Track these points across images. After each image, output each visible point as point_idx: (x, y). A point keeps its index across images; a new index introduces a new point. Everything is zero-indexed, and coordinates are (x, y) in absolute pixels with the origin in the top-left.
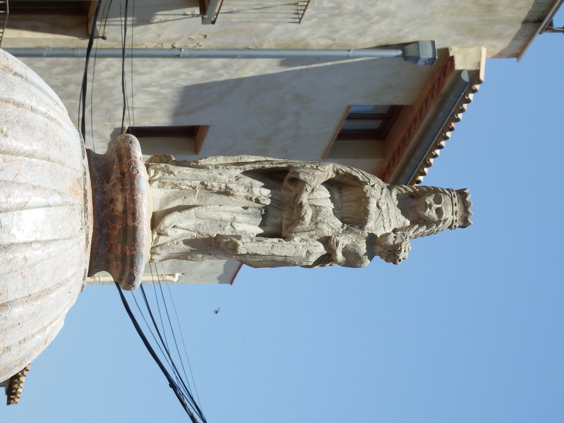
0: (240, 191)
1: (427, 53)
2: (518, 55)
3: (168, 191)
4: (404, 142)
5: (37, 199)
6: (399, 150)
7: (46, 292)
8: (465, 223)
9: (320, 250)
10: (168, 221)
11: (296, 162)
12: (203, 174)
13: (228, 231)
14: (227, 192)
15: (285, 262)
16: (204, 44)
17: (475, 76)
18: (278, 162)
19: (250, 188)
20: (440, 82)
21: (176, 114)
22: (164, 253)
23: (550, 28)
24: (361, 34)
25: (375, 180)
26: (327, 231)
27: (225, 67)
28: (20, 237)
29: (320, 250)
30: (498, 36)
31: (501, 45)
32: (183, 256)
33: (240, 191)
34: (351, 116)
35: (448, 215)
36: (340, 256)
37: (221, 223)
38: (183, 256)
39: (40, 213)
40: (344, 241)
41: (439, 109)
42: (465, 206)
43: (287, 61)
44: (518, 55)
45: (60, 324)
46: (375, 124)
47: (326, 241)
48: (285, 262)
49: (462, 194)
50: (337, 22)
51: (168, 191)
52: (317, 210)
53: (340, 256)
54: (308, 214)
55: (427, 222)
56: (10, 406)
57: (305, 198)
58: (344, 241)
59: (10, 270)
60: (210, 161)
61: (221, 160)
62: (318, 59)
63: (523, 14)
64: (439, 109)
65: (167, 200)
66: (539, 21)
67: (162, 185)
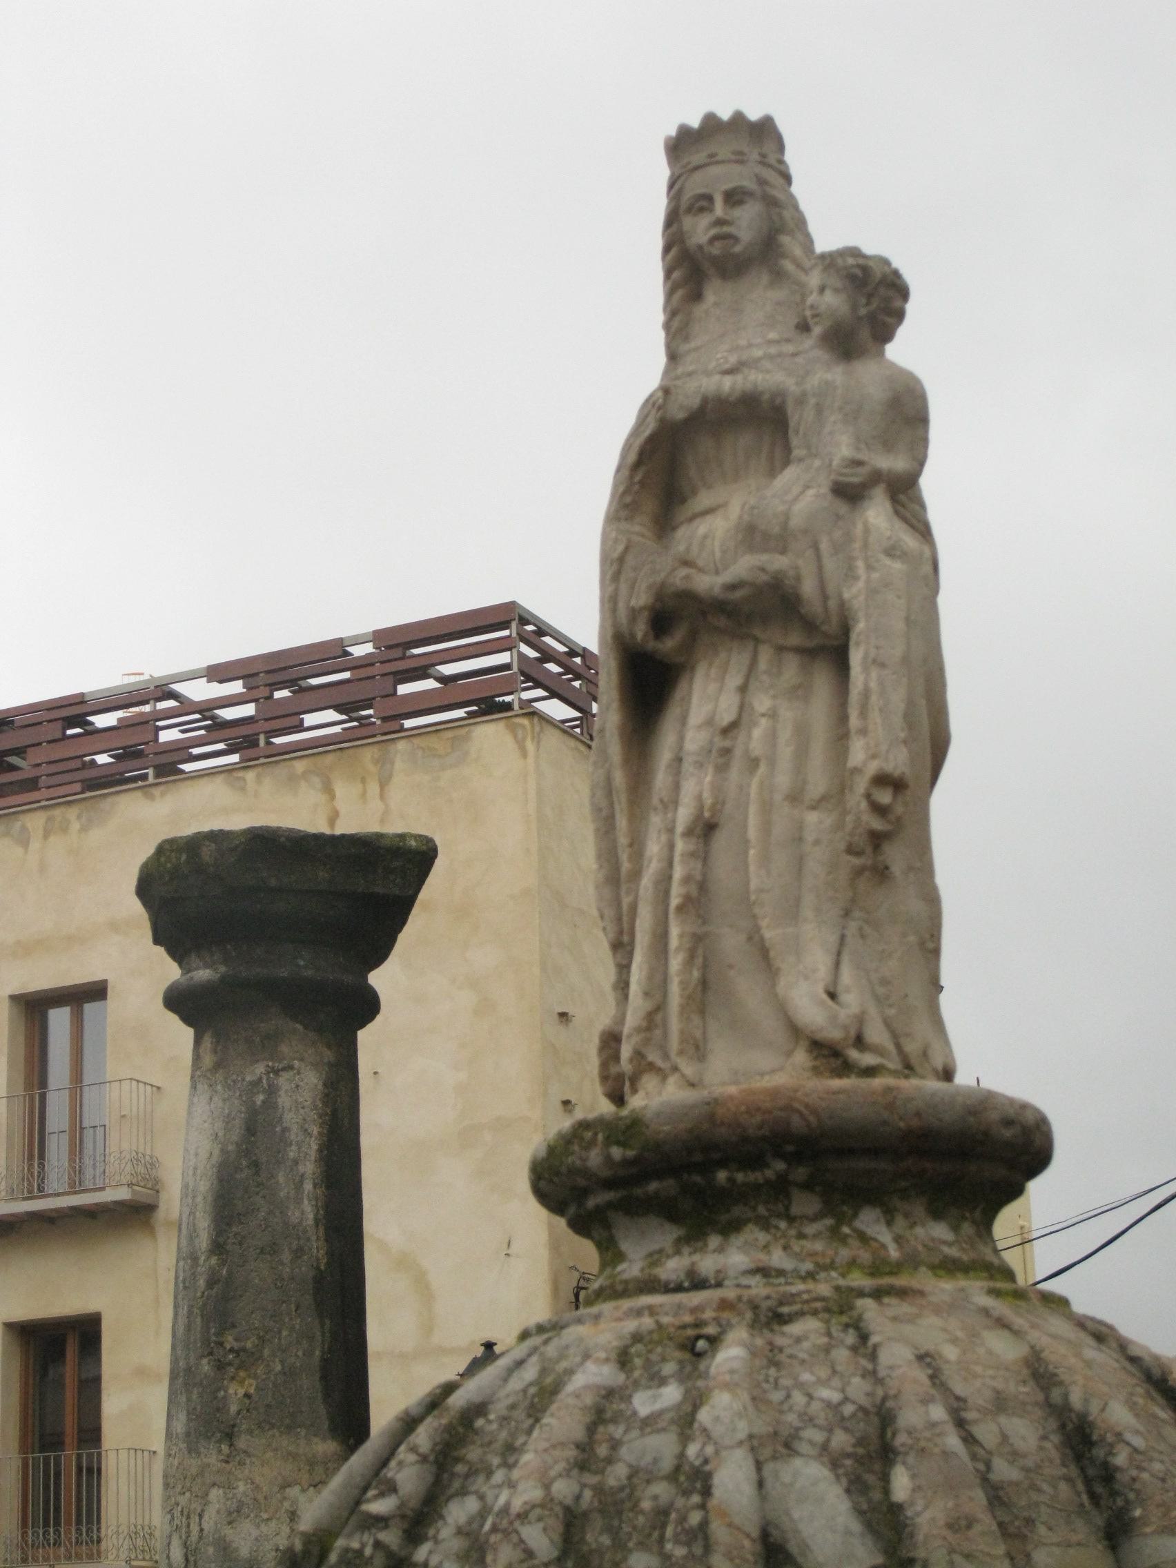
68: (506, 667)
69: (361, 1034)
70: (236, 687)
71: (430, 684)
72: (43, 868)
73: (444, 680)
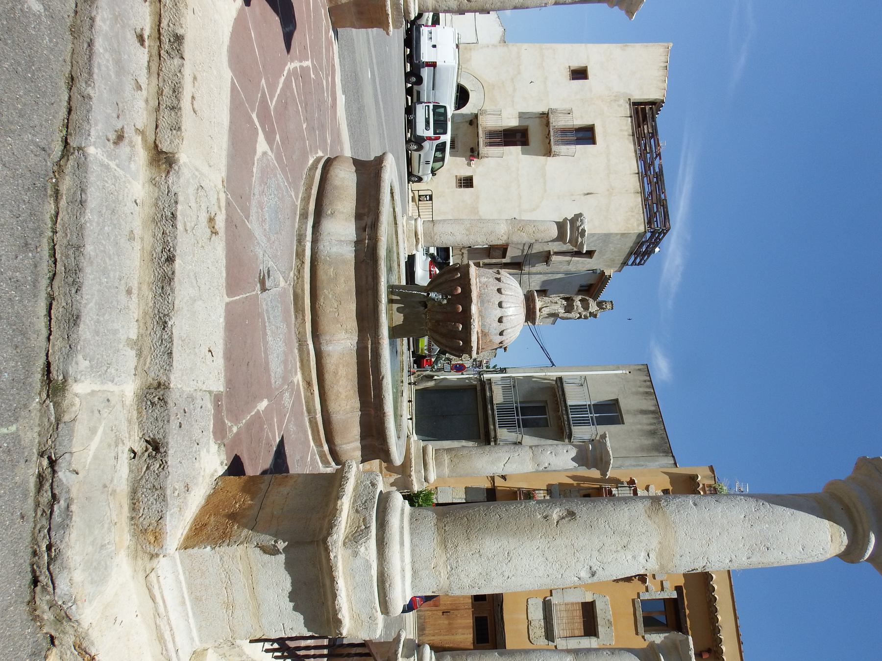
0: (560, 303)
1: (599, 272)
2: (620, 271)
3: (543, 303)
4: (594, 291)
5: (513, 305)
6: (593, 294)
7: (515, 326)
8: (612, 309)
9: (579, 315)
10: (543, 309)
11: (572, 296)
12: (550, 299)
13: (557, 312)
14: (556, 303)
15: (570, 318)
16: (547, 271)
17: (610, 276)
18: (568, 296)
19: (562, 302)
20: (602, 278)
21: (541, 287)
22: (542, 317)
23: (628, 265)
24: (583, 268)
25: (591, 299)
26: (580, 311)
27: (569, 263)
28: (510, 314)
29: (579, 315)
30: (615, 267)
31: (616, 269)
32: (546, 318)
33: (560, 303)
34: (581, 286)
35: (608, 307)
36: (583, 317)
37: (555, 310)
38: (546, 318)
39: (513, 309)
40: (584, 313)
41: (602, 284)
42: (612, 305)
43: (566, 274)
44: (620, 271)
45: (519, 333)
46: (586, 288)
47: (580, 313)
48: (570, 318)
49: (611, 302)
50: (578, 265)
51: (543, 303)
52: (577, 306)
53: (583, 317)
54: (575, 307)
55: (604, 309)
56: (543, 109)
57: (574, 304)
58: (584, 313)
59: (369, 527)
60: (552, 296)
61: (555, 295)
62: (573, 274)
63: (621, 262)
64: (602, 284)
65: (543, 305)
66: (625, 263)
67: (541, 302)
68: (658, 227)
69: (302, 617)
70: (657, 170)
71: (655, 210)
72: (621, 130)
73: (656, 213)
